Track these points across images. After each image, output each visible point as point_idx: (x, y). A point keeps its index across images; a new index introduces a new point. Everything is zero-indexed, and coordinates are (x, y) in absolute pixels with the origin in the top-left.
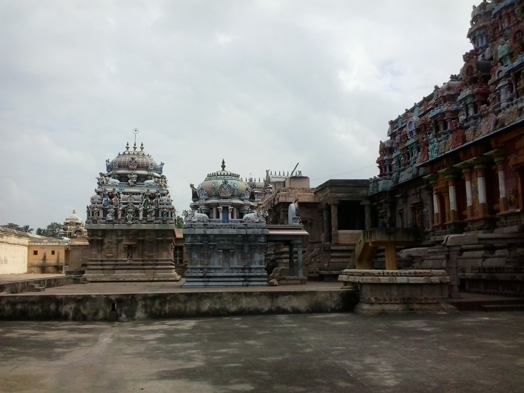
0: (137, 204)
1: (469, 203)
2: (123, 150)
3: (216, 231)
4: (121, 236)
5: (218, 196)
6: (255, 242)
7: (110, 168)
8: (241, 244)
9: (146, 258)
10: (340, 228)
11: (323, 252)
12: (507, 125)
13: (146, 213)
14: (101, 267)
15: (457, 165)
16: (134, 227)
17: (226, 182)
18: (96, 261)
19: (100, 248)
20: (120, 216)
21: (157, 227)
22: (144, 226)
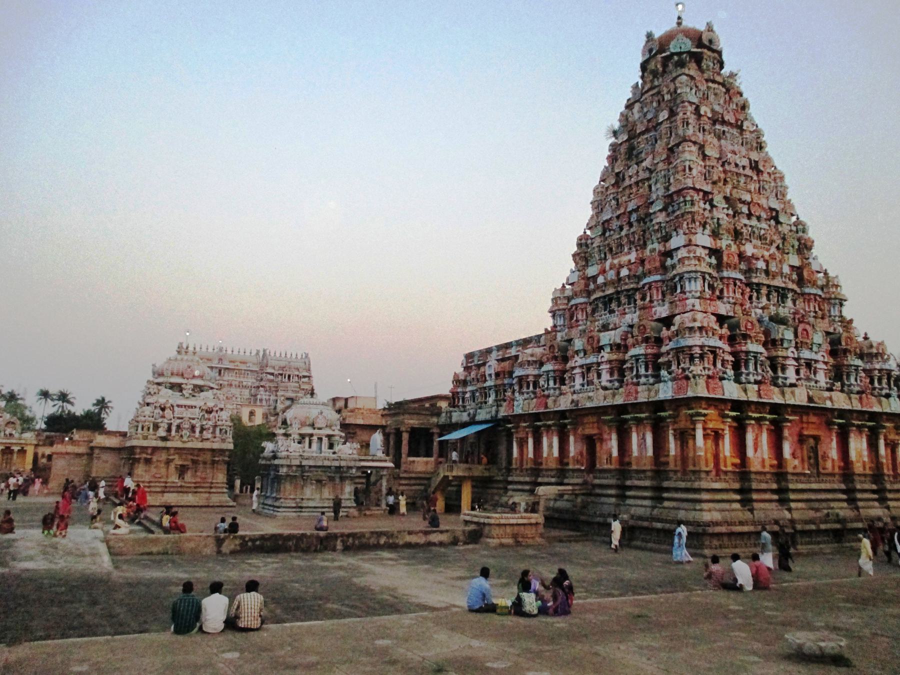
0: (193, 419)
1: (545, 455)
3: (311, 463)
4: (174, 455)
5: (312, 425)
8: (333, 475)
9: (199, 480)
10: (409, 455)
12: (580, 406)
13: (202, 429)
15: (538, 423)
16: (189, 445)
20: (173, 433)
21: (216, 446)
22: (200, 445)
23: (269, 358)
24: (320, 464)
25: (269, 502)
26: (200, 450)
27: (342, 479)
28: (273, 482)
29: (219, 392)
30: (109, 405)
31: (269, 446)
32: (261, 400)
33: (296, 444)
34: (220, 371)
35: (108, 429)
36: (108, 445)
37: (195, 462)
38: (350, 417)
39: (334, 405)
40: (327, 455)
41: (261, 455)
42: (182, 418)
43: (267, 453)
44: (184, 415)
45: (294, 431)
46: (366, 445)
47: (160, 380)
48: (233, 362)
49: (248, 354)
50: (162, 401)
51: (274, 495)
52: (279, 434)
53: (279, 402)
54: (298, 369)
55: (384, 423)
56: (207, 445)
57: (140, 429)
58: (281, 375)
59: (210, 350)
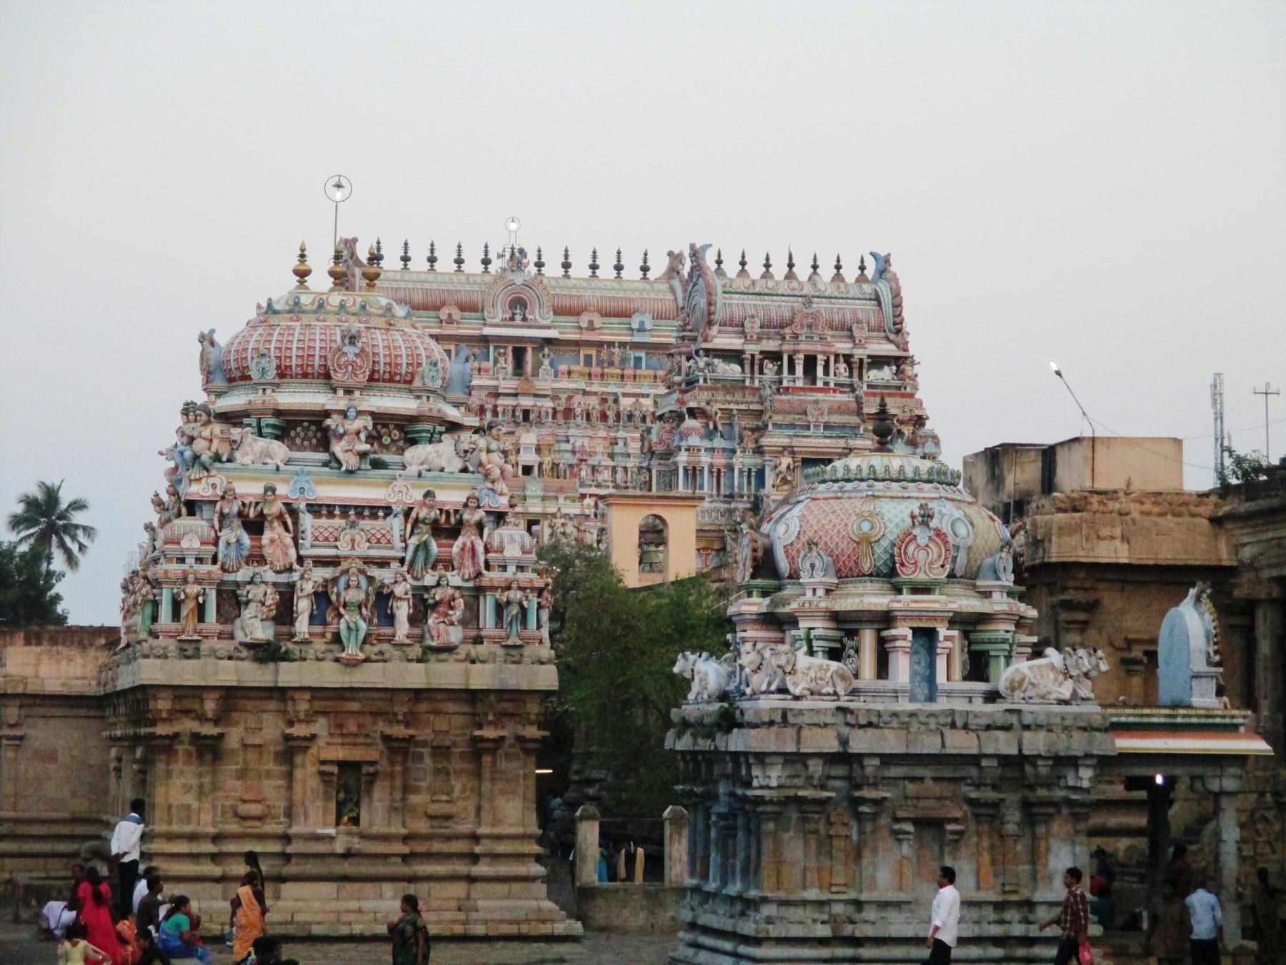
0: (383, 563)
2: (282, 287)
3: (891, 743)
4: (309, 719)
5: (889, 575)
6: (1048, 785)
7: (225, 371)
8: (990, 795)
9: (422, 826)
11: (1270, 815)
13: (423, 607)
14: (217, 871)
16: (371, 676)
17: (926, 517)
18: (193, 837)
19: (207, 780)
20: (302, 625)
21: (481, 678)
22: (415, 676)
23: (718, 284)
24: (929, 745)
25: (716, 918)
26: (418, 694)
27: (1034, 814)
28: (728, 833)
29: (482, 442)
30: (78, 518)
31: (705, 672)
32: (693, 473)
33: (820, 660)
34: (519, 355)
35: (72, 621)
36: (53, 687)
37: (399, 749)
38: (1065, 530)
39: (996, 479)
40: (959, 705)
41: (675, 714)
42: (333, 562)
43: (697, 705)
44: (344, 549)
45: (810, 597)
46: (1140, 661)
47: (235, 401)
48: (575, 312)
49: (632, 272)
50: (250, 489)
51: (734, 888)
52: (742, 618)
53: (770, 479)
54: (847, 330)
55: (1225, 557)
56: (447, 674)
57: (165, 611)
58: (775, 356)
59: (473, 266)
